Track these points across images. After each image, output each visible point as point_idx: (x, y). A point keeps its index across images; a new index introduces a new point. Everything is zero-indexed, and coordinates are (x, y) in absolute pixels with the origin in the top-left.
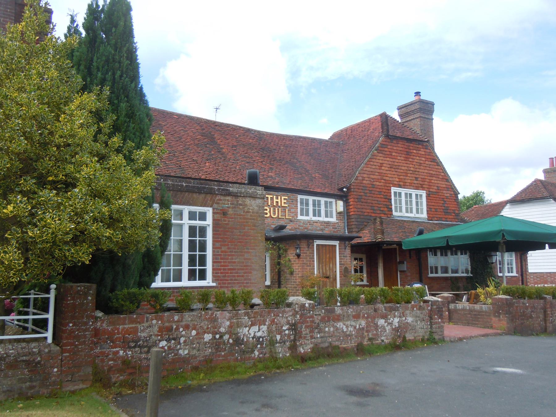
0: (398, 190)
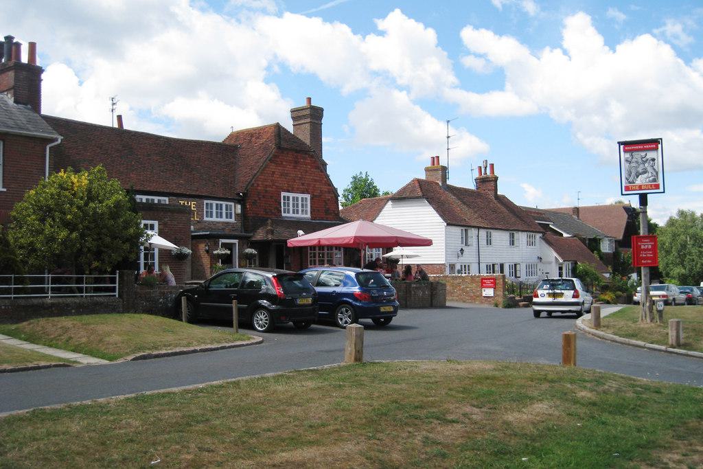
0: (287, 194)
